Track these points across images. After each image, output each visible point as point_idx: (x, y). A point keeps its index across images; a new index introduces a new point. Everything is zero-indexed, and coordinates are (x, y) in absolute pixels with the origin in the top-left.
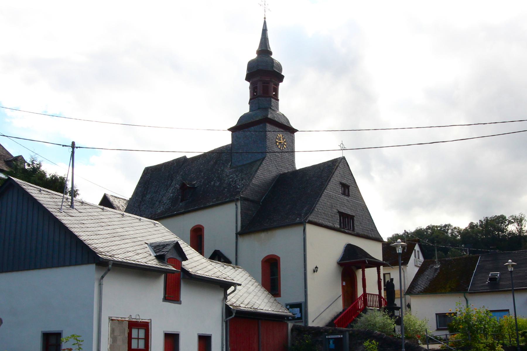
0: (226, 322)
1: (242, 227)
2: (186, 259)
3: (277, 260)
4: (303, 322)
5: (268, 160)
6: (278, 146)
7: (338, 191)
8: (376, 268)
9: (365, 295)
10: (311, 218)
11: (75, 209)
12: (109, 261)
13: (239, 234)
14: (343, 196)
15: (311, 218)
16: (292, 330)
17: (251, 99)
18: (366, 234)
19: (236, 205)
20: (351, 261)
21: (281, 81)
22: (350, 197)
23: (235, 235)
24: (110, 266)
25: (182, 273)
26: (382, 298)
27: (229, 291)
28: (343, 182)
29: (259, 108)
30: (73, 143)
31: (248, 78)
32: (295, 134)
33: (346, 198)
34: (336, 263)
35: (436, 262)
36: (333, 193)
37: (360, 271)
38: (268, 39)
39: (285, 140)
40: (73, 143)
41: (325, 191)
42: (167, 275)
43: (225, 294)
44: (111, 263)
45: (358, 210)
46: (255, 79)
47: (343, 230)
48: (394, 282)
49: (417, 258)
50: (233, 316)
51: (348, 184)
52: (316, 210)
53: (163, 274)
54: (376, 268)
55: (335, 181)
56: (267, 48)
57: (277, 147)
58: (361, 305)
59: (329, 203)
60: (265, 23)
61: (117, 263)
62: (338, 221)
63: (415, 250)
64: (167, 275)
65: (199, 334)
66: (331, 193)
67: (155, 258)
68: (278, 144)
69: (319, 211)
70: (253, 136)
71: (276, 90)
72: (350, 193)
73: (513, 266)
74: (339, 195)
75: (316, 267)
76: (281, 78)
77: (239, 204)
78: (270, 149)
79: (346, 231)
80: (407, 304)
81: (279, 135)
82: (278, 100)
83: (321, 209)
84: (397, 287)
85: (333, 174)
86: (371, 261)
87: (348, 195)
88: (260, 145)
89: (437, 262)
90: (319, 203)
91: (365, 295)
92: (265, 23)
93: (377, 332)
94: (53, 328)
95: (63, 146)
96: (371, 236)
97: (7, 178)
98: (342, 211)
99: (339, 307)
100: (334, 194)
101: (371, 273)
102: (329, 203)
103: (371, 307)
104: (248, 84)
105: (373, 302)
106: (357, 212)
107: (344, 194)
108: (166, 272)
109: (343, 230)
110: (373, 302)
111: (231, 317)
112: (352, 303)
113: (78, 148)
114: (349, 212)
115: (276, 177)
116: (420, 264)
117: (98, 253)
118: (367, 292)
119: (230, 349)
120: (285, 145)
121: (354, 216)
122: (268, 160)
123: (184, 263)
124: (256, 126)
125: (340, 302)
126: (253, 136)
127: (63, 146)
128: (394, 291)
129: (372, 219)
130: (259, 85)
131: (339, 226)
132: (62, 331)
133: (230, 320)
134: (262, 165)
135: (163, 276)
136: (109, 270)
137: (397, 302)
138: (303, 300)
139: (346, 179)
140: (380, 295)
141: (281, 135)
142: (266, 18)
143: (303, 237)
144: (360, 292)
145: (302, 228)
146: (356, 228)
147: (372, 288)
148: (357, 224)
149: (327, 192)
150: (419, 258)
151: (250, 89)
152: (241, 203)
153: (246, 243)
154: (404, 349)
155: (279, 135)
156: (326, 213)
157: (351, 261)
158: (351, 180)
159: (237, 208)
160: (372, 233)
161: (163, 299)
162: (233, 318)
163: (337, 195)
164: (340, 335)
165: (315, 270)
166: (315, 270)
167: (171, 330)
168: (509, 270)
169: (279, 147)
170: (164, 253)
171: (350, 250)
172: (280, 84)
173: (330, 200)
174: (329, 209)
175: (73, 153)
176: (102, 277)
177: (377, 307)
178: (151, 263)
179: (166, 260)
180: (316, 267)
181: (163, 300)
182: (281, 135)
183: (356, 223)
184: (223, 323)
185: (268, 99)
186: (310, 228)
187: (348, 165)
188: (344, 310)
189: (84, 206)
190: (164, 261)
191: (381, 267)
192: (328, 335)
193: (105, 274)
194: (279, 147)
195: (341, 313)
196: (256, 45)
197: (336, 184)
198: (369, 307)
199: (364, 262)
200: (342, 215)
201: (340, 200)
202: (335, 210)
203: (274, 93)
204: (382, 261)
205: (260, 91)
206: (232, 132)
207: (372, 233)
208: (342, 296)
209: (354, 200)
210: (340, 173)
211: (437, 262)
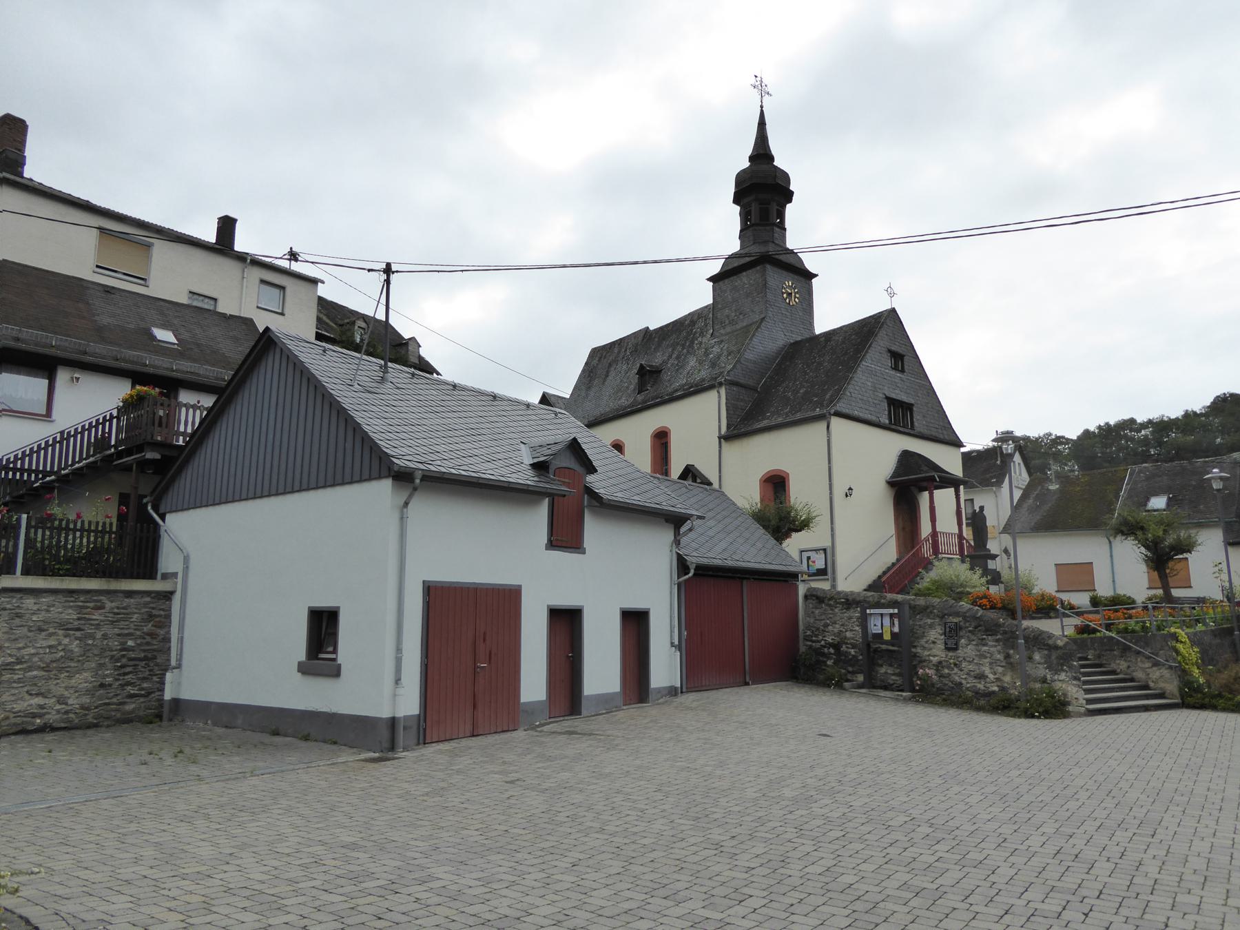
0: (679, 585)
1: (728, 426)
2: (592, 469)
3: (784, 479)
4: (828, 579)
5: (769, 321)
6: (785, 300)
7: (885, 363)
8: (952, 490)
9: (934, 534)
10: (841, 406)
11: (391, 382)
12: (414, 472)
13: (726, 438)
14: (893, 372)
15: (841, 406)
16: (806, 597)
17: (741, 231)
18: (934, 434)
19: (718, 392)
20: (910, 477)
21: (790, 201)
22: (905, 374)
23: (717, 439)
24: (418, 481)
25: (586, 496)
26: (965, 538)
27: (683, 530)
28: (893, 348)
29: (754, 243)
30: (389, 265)
31: (737, 200)
32: (813, 280)
33: (898, 375)
34: (884, 482)
35: (1051, 479)
36: (876, 367)
37: (926, 494)
38: (767, 138)
39: (796, 290)
40: (389, 265)
41: (864, 363)
42: (553, 499)
43: (677, 534)
44: (418, 475)
45: (919, 395)
46: (746, 200)
47: (893, 427)
48: (794, 535)
49: (1018, 474)
50: (691, 575)
51: (901, 352)
52: (849, 394)
53: (544, 499)
54: (952, 490)
55: (879, 347)
56: (766, 150)
57: (784, 301)
58: (927, 551)
59: (869, 384)
60: (762, 124)
61: (497, 484)
62: (886, 413)
63: (1014, 462)
64: (553, 499)
65: (623, 608)
66: (873, 366)
67: (530, 468)
68: (785, 295)
69: (853, 395)
70: (747, 286)
71: (781, 215)
72: (906, 367)
73: (1221, 478)
74: (887, 371)
75: (850, 489)
76: (788, 196)
77: (723, 391)
78: (772, 303)
79: (901, 429)
80: (1003, 549)
81: (786, 283)
82: (785, 229)
83: (856, 392)
84: (990, 522)
85: (876, 335)
86: (944, 478)
87: (903, 371)
88: (757, 299)
89: (1054, 480)
90: (853, 382)
91: (934, 534)
92: (762, 124)
93: (963, 605)
94: (324, 601)
95: (369, 270)
96: (941, 437)
97: (923, 539)
98: (893, 396)
99: (890, 554)
100: (878, 368)
101: (945, 498)
102: (869, 384)
103: (945, 553)
104: (737, 208)
105: (949, 546)
106: (917, 398)
107: (895, 368)
108: (553, 496)
109: (893, 427)
110: (949, 546)
111: (687, 577)
112: (913, 547)
113: (395, 274)
114: (903, 397)
115: (783, 349)
116: (1022, 485)
117: (393, 456)
118: (938, 529)
119: (686, 633)
120: (798, 298)
121: (912, 405)
122: (769, 321)
123: (590, 478)
124: (750, 271)
125: (893, 544)
126: (747, 286)
127: (369, 270)
128: (987, 527)
129: (943, 409)
130: (754, 208)
131: (887, 422)
132: (339, 608)
133: (686, 581)
134: (759, 330)
135: (546, 501)
136: (415, 489)
137: (993, 546)
138: (830, 544)
139: (897, 344)
140: (960, 536)
141: (790, 283)
142: (764, 106)
143: (826, 439)
144: (925, 529)
145: (823, 425)
146: (916, 424)
147: (947, 523)
148: (918, 417)
149: (866, 364)
150: (1020, 474)
151: (740, 216)
152: (726, 389)
153: (734, 451)
154: (1023, 641)
155: (786, 283)
156: (865, 398)
157: (910, 477)
158: (906, 345)
159: (719, 397)
160: (945, 432)
161: (546, 545)
162: (689, 578)
163: (883, 369)
164: (894, 608)
165: (849, 493)
166: (849, 493)
167: (565, 601)
168: (1215, 488)
169: (787, 301)
170: (546, 458)
171: (908, 460)
172: (788, 206)
173: (872, 378)
174: (871, 392)
175: (388, 282)
176: (406, 504)
177: (956, 554)
178: (517, 476)
179: (551, 471)
180: (850, 489)
181: (546, 547)
182: (790, 283)
183: (917, 417)
184: (673, 587)
185: (768, 228)
186: (836, 422)
187: (901, 322)
188: (898, 560)
189: (415, 379)
190: (548, 473)
191: (962, 487)
192: (870, 608)
193: (410, 497)
194: (787, 301)
195: (893, 564)
196: (747, 147)
197: (881, 351)
198: (942, 553)
199: (932, 479)
200: (893, 403)
201: (889, 378)
202: (881, 395)
203: (778, 220)
204: (962, 476)
205: (754, 218)
206: (714, 283)
207: (945, 432)
208: (894, 536)
209: (913, 379)
210: (887, 335)
211: (1054, 480)
